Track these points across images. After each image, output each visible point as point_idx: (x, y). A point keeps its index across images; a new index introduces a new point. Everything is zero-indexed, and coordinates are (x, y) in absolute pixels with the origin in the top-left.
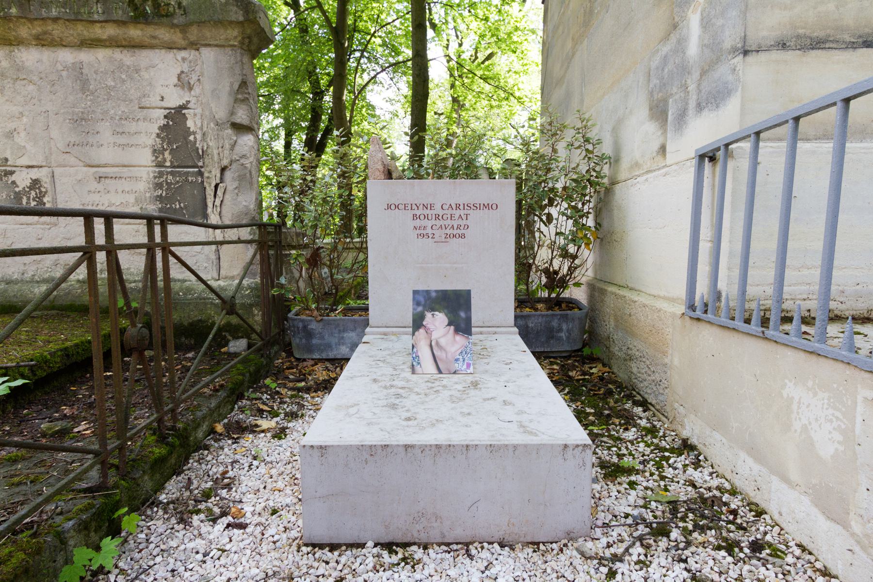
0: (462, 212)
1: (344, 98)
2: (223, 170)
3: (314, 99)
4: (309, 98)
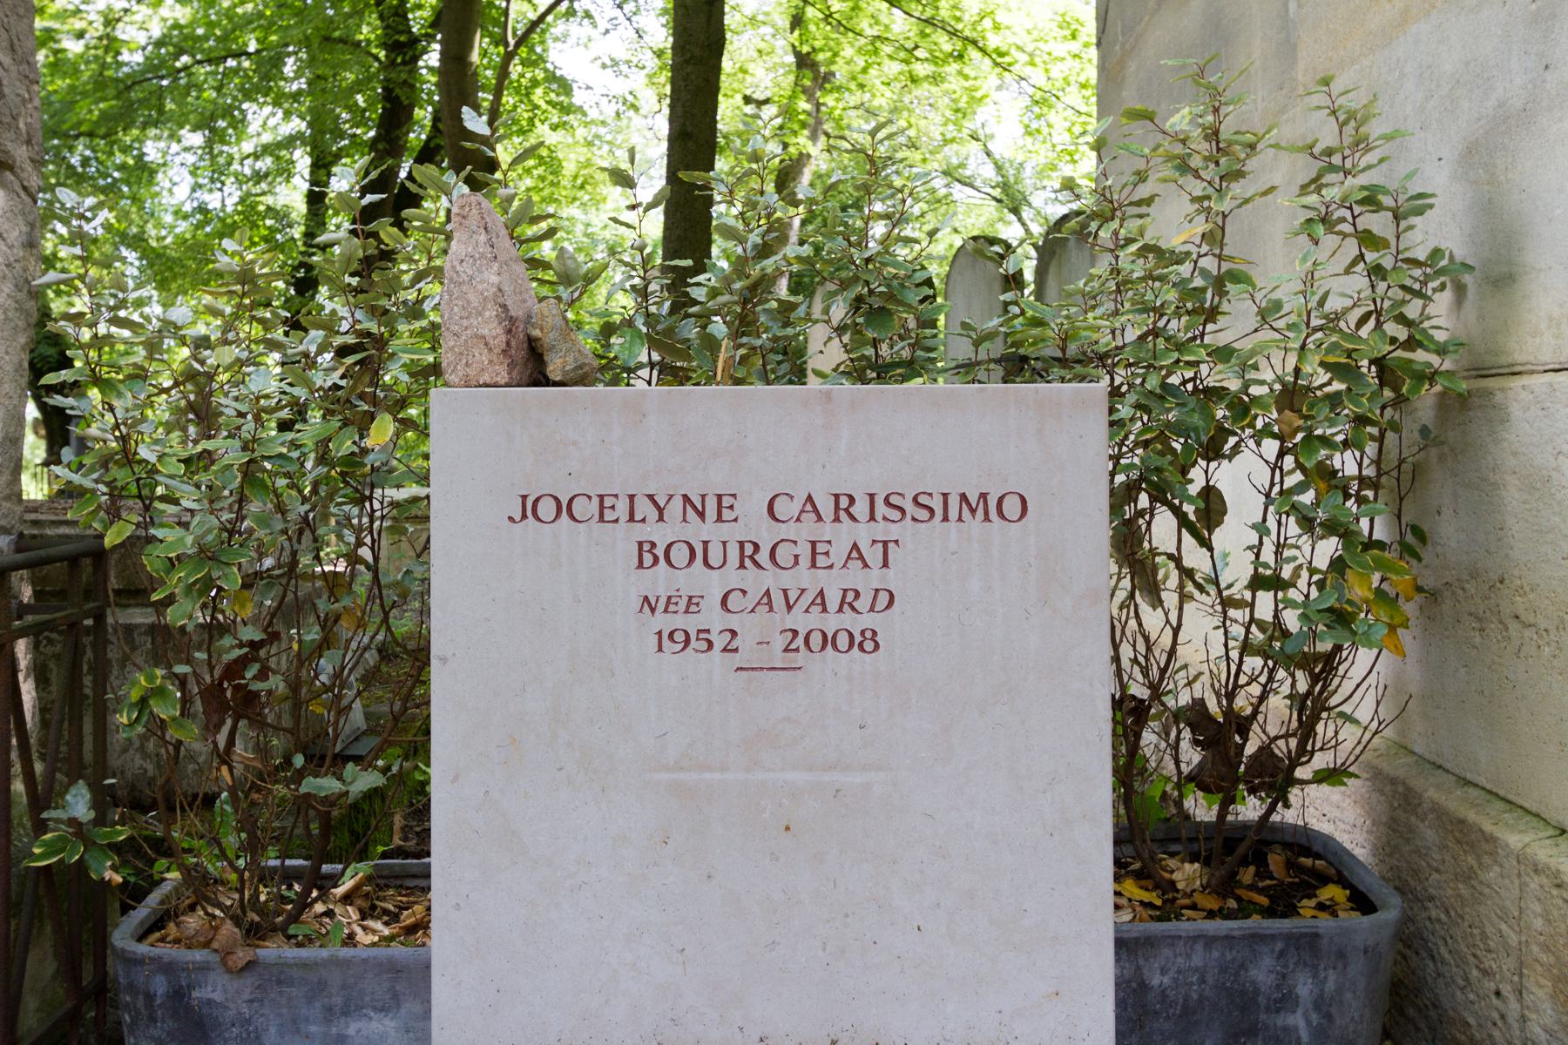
0: (864, 533)
1: (475, 57)
3: (391, 64)
4: (376, 58)
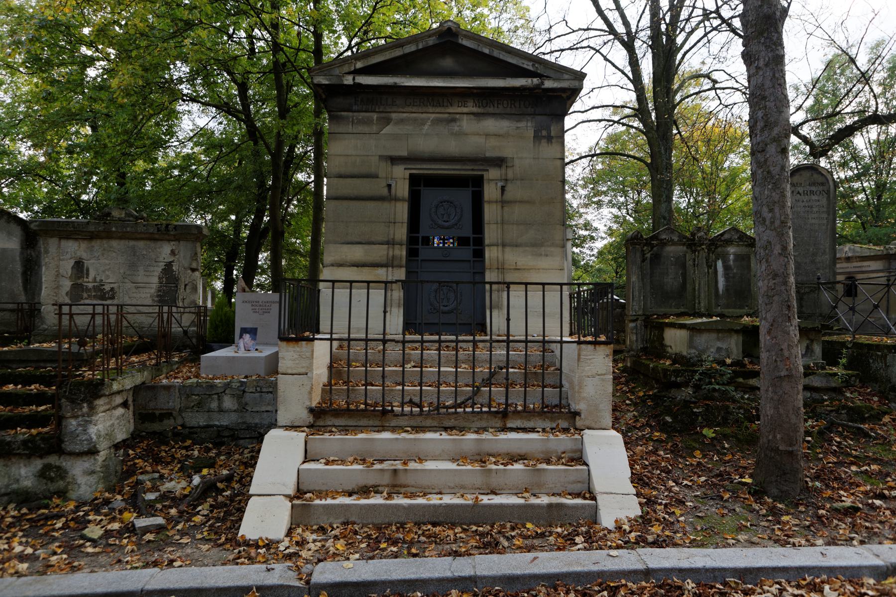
2: (186, 285)
